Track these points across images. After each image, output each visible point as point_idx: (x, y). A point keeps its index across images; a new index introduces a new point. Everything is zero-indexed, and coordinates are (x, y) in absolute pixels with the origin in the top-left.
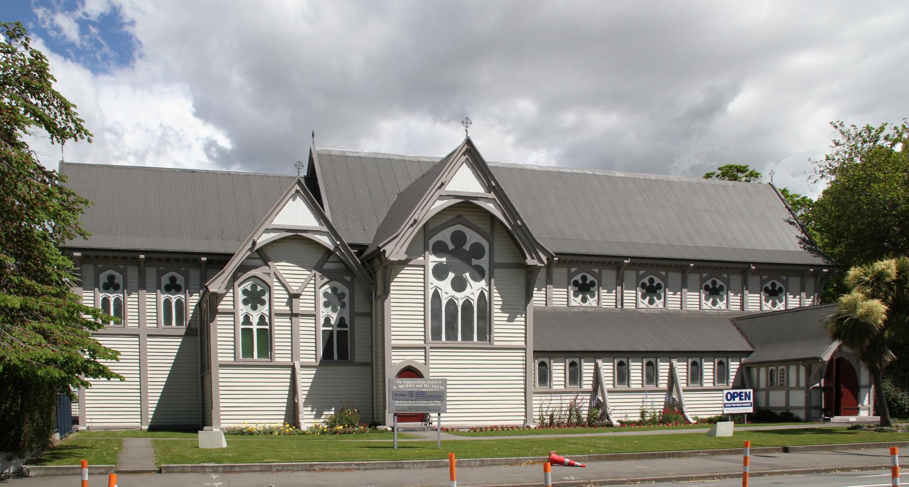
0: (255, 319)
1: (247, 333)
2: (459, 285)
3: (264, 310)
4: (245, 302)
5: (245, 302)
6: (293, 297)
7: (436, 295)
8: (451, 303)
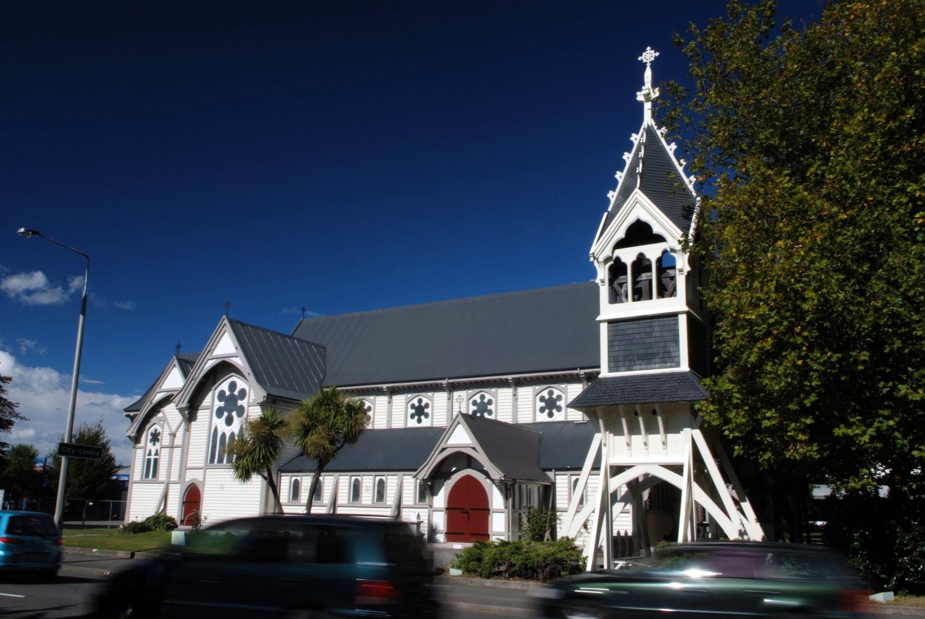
0: (153, 452)
1: (149, 460)
2: (229, 421)
3: (158, 445)
4: (151, 441)
5: (151, 441)
6: (174, 435)
7: (216, 430)
8: (224, 435)
